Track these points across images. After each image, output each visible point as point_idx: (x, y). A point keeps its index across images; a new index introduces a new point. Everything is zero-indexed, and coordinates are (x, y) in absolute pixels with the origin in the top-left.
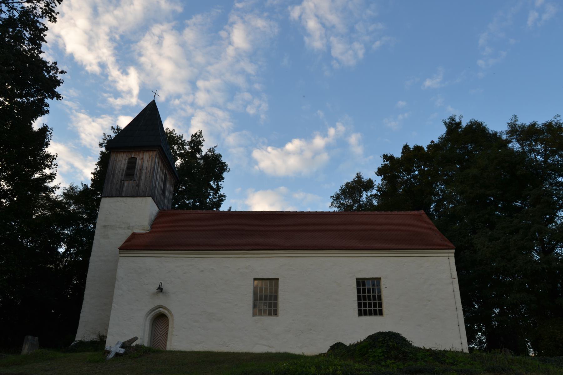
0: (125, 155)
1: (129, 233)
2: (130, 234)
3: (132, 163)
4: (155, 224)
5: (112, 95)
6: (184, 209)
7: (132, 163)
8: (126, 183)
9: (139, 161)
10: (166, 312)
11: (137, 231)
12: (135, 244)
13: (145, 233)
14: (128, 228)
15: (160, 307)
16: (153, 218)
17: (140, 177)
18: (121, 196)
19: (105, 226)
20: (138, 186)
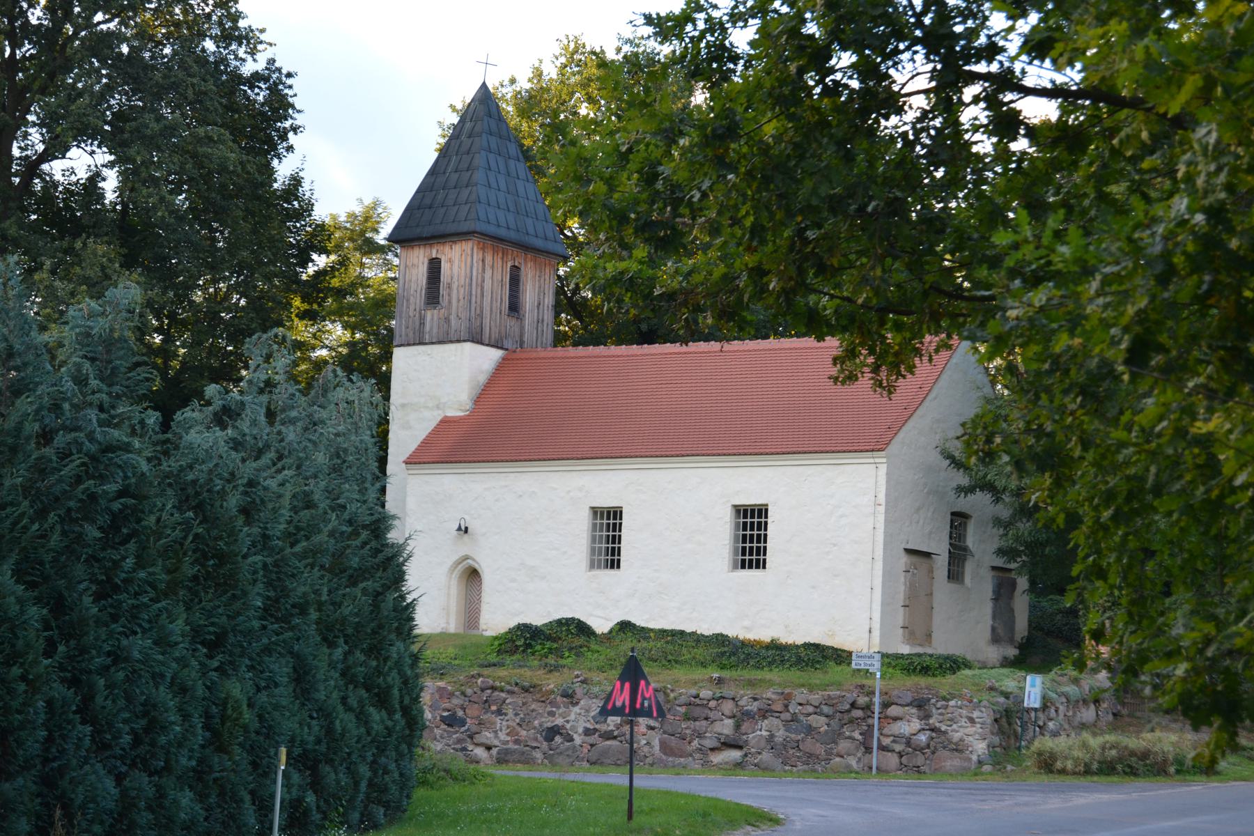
0: (422, 251)
1: (437, 416)
2: (439, 418)
3: (434, 267)
4: (484, 395)
5: (966, 294)
6: (766, 337)
7: (434, 267)
8: (429, 314)
9: (445, 266)
10: (476, 566)
11: (451, 413)
12: (454, 445)
13: (461, 418)
14: (438, 407)
15: (467, 558)
16: (483, 379)
17: (450, 302)
18: (421, 343)
19: (403, 406)
20: (447, 320)
